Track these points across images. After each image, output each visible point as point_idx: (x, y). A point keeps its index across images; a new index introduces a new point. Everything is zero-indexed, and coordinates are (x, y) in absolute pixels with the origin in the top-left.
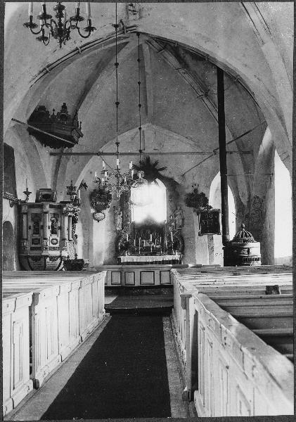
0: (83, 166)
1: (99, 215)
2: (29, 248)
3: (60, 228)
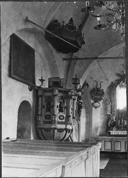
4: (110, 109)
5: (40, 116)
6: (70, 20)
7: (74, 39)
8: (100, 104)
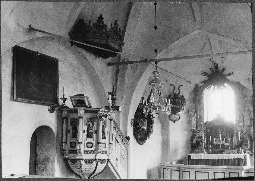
0: (141, 74)
1: (175, 117)
2: (67, 152)
3: (96, 132)
4: (195, 123)
5: (64, 144)
6: (99, 18)
7: (104, 42)
8: (179, 116)
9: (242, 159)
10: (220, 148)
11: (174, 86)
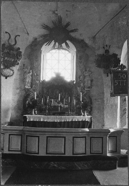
8: (13, 71)
9: (88, 122)
10: (58, 110)
11: (9, 34)
